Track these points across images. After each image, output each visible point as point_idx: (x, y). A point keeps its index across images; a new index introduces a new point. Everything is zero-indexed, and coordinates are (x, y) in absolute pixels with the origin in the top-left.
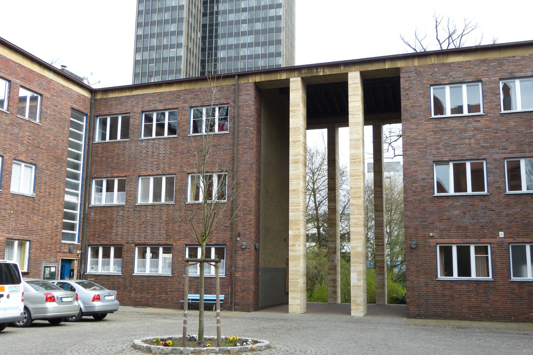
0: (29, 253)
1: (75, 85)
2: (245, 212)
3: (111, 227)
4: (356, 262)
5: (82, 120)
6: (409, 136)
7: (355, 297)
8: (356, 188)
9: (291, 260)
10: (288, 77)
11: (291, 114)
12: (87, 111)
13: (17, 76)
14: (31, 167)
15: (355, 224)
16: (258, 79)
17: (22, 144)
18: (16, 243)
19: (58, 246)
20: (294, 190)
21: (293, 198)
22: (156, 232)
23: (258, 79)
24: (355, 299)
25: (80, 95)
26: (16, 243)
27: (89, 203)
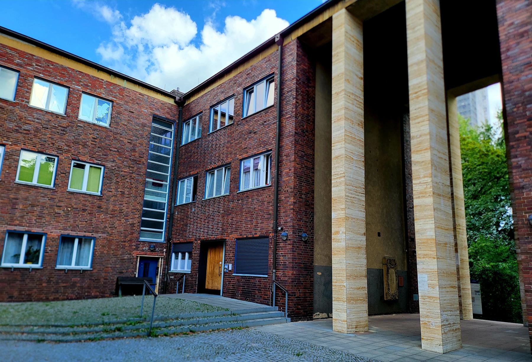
0: (94, 249)
1: (52, 54)
2: (286, 195)
3: (186, 225)
4: (425, 256)
5: (171, 128)
6: (512, 24)
7: (427, 316)
8: (421, 136)
9: (335, 254)
10: (330, 16)
11: (334, 60)
12: (176, 118)
13: (78, 82)
14: (101, 168)
15: (421, 193)
16: (300, 32)
17: (85, 145)
18: (76, 241)
19: (133, 244)
20: (337, 157)
21: (336, 168)
22: (215, 226)
23: (300, 32)
24: (427, 319)
25: (163, 104)
26: (76, 241)
27: (175, 203)
